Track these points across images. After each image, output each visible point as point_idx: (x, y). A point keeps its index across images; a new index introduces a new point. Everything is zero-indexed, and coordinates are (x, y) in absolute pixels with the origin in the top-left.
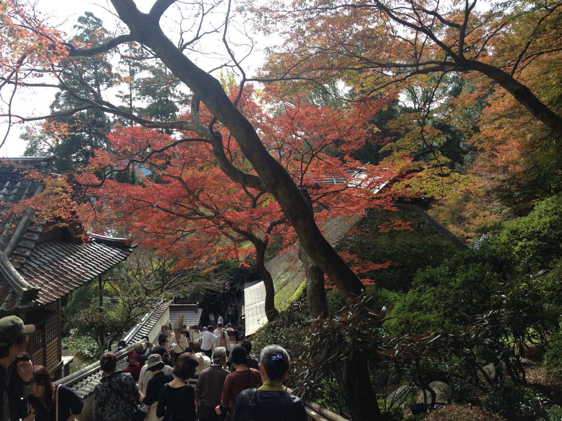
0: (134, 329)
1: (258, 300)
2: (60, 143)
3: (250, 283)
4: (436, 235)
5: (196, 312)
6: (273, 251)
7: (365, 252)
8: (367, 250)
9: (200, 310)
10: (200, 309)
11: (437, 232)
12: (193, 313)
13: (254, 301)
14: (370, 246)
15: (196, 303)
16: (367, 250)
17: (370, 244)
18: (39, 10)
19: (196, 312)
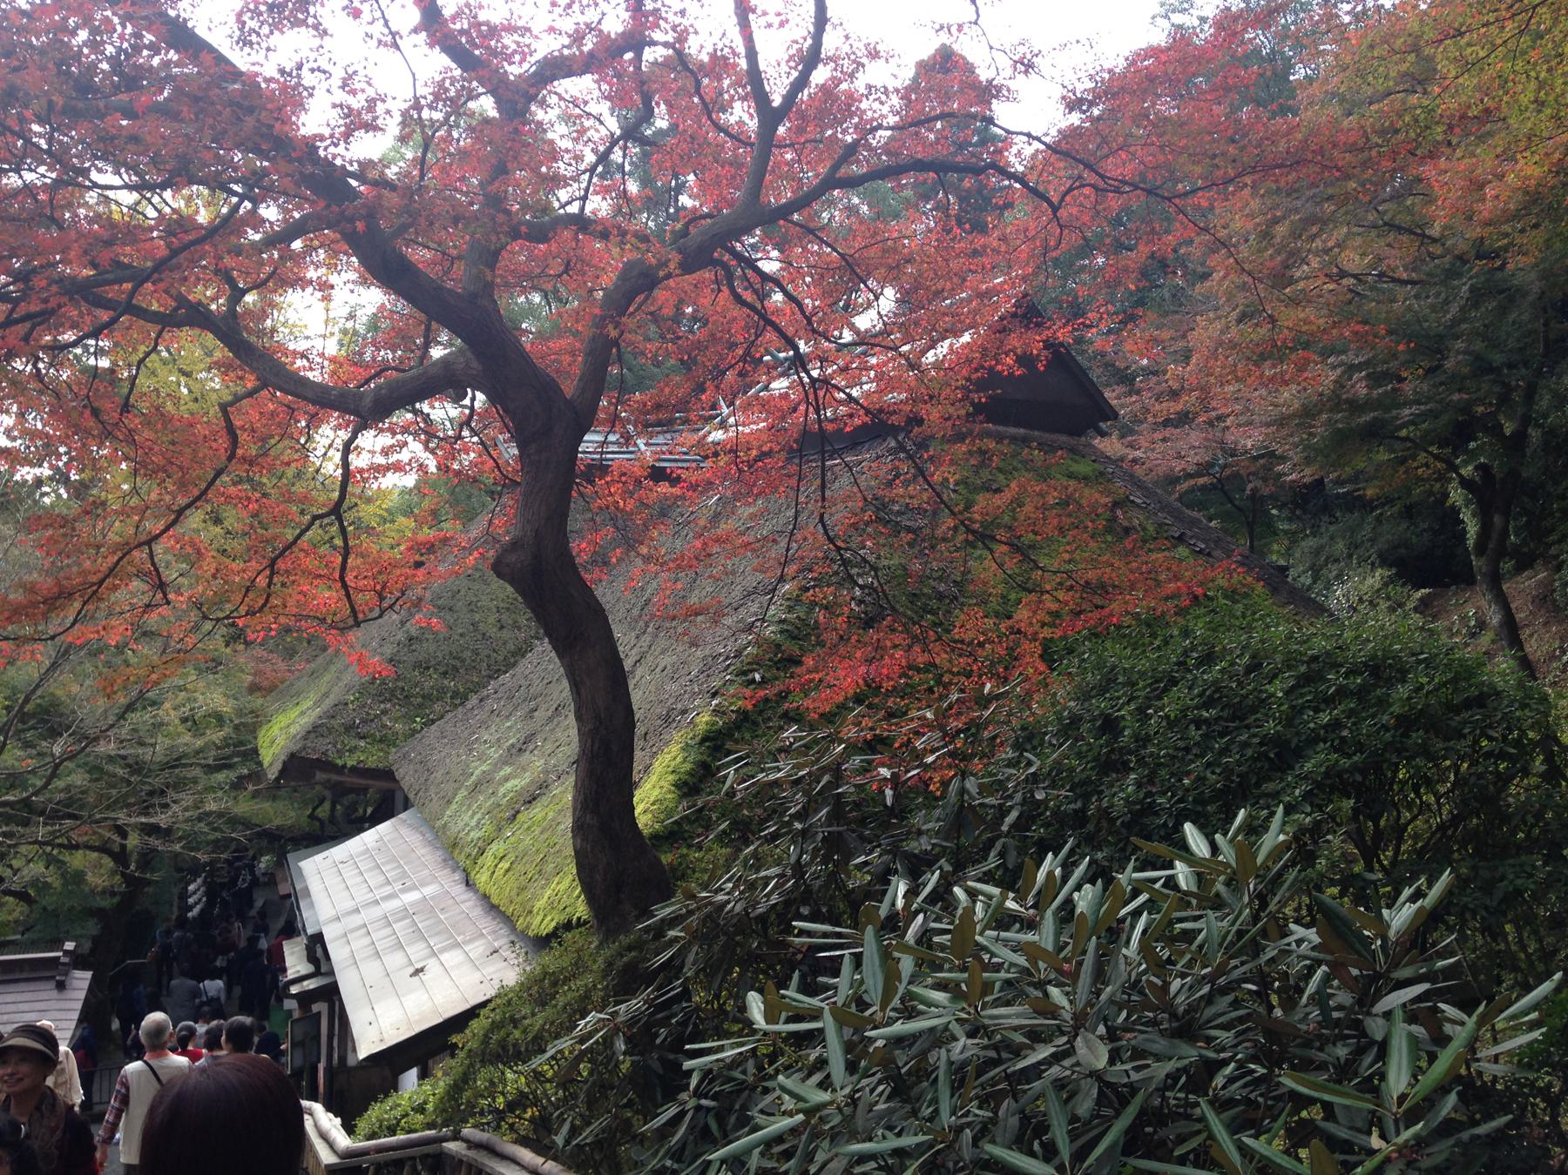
0: (1022, 431)
1: (387, 890)
2: (214, 307)
3: (303, 852)
4: (1182, 551)
5: (61, 986)
6: (420, 706)
7: (926, 610)
8: (934, 603)
9: (82, 980)
10: (78, 974)
11: (1181, 539)
12: (47, 992)
13: (362, 896)
14: (942, 587)
15: (59, 947)
16: (934, 603)
17: (940, 579)
18: (677, 7)
19: (61, 986)
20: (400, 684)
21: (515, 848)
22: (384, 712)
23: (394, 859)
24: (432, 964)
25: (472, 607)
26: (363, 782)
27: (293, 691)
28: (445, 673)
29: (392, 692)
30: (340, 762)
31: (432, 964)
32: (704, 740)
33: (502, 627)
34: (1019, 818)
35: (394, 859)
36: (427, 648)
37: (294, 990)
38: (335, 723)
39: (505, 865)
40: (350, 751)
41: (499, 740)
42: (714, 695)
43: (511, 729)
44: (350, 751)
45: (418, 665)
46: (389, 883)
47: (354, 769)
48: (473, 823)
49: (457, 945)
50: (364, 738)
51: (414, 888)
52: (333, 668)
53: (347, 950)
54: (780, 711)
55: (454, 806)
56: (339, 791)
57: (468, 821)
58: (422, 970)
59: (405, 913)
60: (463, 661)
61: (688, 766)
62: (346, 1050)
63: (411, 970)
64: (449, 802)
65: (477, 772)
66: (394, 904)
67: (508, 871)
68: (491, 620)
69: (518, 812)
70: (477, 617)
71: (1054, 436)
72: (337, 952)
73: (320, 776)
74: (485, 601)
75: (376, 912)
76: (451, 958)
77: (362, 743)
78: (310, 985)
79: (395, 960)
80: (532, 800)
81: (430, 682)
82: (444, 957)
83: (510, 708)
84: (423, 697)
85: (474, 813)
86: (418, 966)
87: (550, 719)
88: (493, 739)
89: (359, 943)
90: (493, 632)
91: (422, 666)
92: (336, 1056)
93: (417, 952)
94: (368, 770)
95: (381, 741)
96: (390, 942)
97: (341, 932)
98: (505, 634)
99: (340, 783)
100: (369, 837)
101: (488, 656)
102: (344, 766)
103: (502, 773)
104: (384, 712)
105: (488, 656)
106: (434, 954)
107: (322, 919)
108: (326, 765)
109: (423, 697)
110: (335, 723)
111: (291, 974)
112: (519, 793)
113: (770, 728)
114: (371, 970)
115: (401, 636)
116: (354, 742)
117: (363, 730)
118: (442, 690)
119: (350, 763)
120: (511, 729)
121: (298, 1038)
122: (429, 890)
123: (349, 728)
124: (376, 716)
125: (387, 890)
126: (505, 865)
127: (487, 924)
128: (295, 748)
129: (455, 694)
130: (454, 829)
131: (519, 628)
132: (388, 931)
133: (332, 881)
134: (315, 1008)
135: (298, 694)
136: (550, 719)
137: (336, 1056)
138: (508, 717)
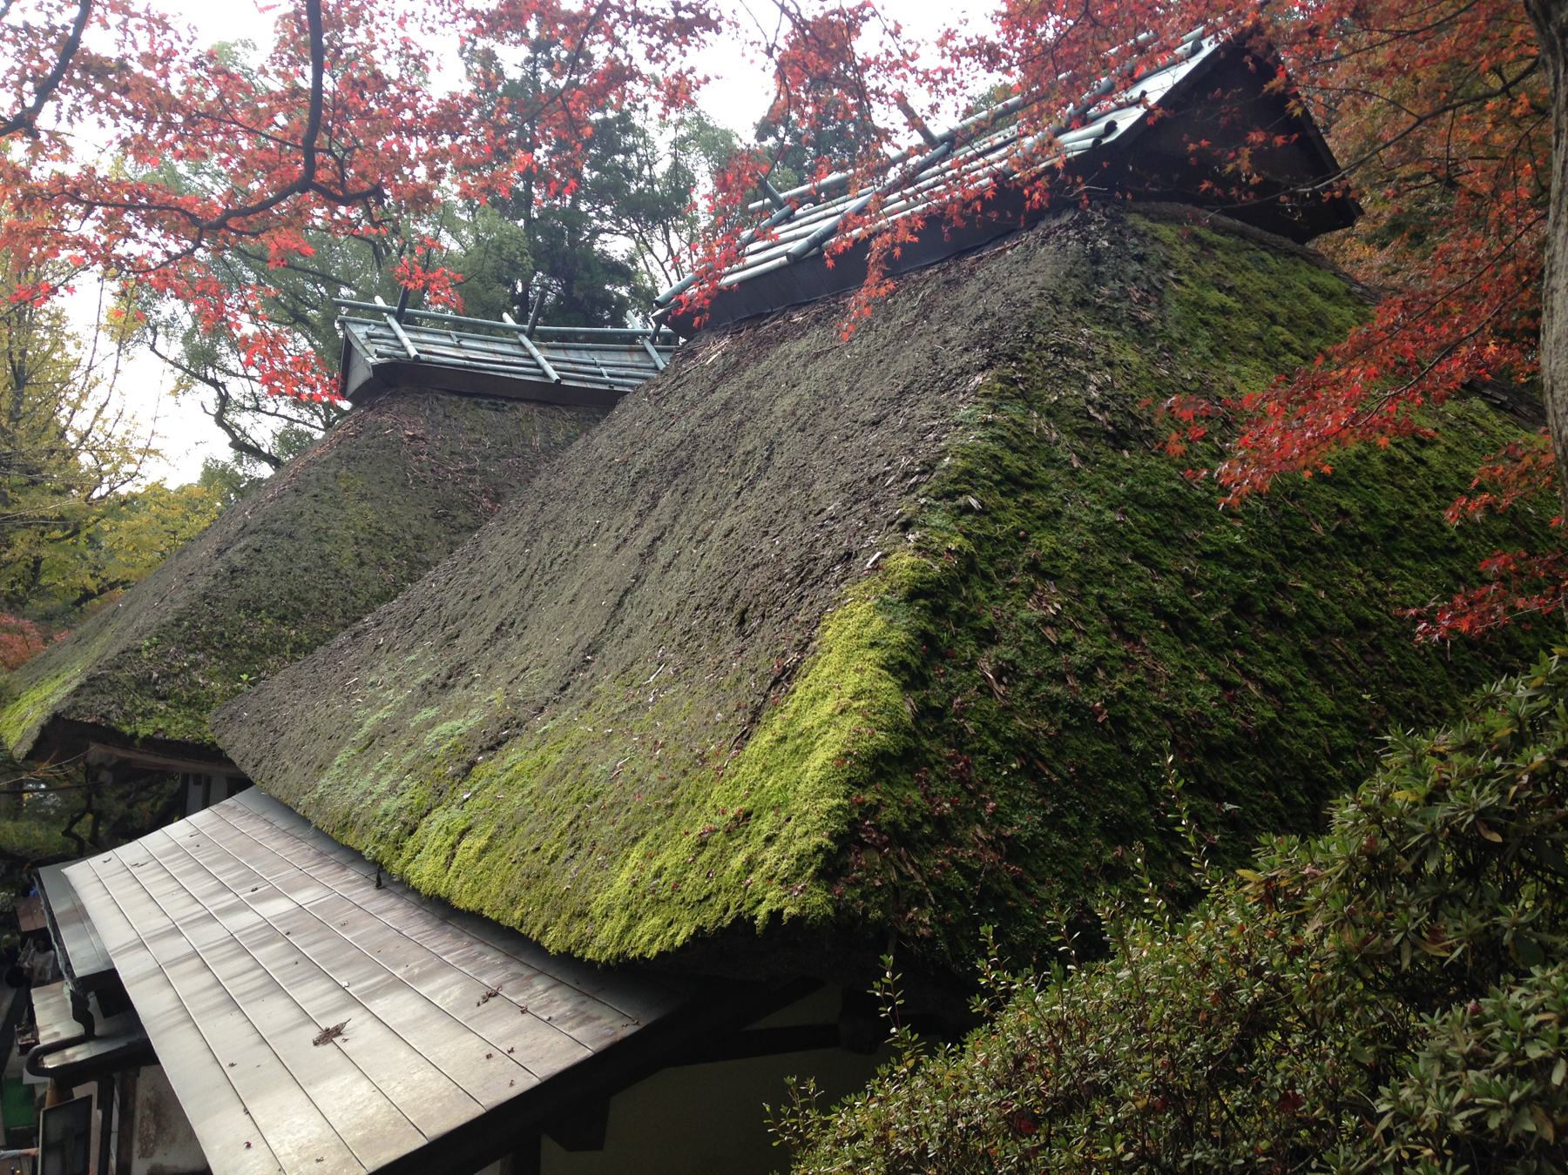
1: (227, 900)
6: (247, 659)
20: (218, 628)
21: (493, 815)
22: (195, 665)
23: (227, 856)
24: (355, 1020)
25: (320, 536)
26: (160, 760)
27: (51, 662)
28: (283, 619)
29: (207, 638)
30: (127, 730)
31: (355, 1020)
32: (912, 596)
33: (362, 564)
34: (99, 999)
35: (227, 856)
36: (254, 585)
37: (51, 1062)
38: (122, 675)
39: (475, 842)
40: (143, 714)
41: (398, 679)
42: (906, 526)
43: (425, 663)
44: (143, 714)
45: (244, 605)
46: (225, 888)
47: (148, 740)
48: (384, 785)
49: (399, 984)
50: (164, 698)
51: (275, 894)
52: (108, 631)
53: (168, 995)
54: (1022, 560)
55: (334, 772)
56: (126, 773)
57: (370, 789)
58: (338, 1031)
59: (270, 932)
60: (308, 604)
61: (899, 636)
62: (130, 1155)
63: (314, 1033)
64: (322, 768)
65: (372, 720)
66: (243, 920)
67: (484, 851)
68: (348, 553)
69: (473, 764)
70: (328, 548)
71: (1279, 238)
72: (148, 1001)
73: (95, 751)
74: (338, 529)
75: (212, 933)
76: (397, 1007)
77: (162, 706)
78: (78, 1054)
79: (272, 1014)
80: (495, 745)
81: (263, 628)
82: (379, 1006)
83: (410, 638)
84: (251, 647)
85: (379, 776)
86: (330, 1024)
87: (490, 642)
88: (389, 678)
89: (190, 984)
90: (349, 568)
91: (252, 607)
92: (113, 1162)
93: (314, 996)
94: (170, 742)
95: (189, 704)
96: (253, 980)
97: (151, 965)
98: (367, 572)
99: (128, 761)
100: (178, 830)
101: (344, 600)
102: (135, 735)
103: (418, 718)
104: (195, 665)
105: (344, 600)
106: (354, 1002)
107: (111, 946)
108: (107, 734)
109: (251, 647)
110: (122, 675)
111: (45, 1038)
112: (468, 737)
113: (1014, 586)
114: (225, 1031)
115: (219, 566)
116: (150, 703)
117: (163, 688)
118: (279, 641)
119: (144, 731)
120: (425, 663)
121: (55, 1136)
122: (306, 897)
123: (143, 683)
124: (183, 670)
125: (227, 900)
126: (475, 842)
127: (448, 945)
128: (60, 709)
129: (298, 647)
130: (340, 804)
131: (386, 567)
132: (242, 963)
133: (123, 890)
134: (79, 1092)
135: (58, 665)
136: (490, 642)
137: (113, 1162)
138: (407, 651)
